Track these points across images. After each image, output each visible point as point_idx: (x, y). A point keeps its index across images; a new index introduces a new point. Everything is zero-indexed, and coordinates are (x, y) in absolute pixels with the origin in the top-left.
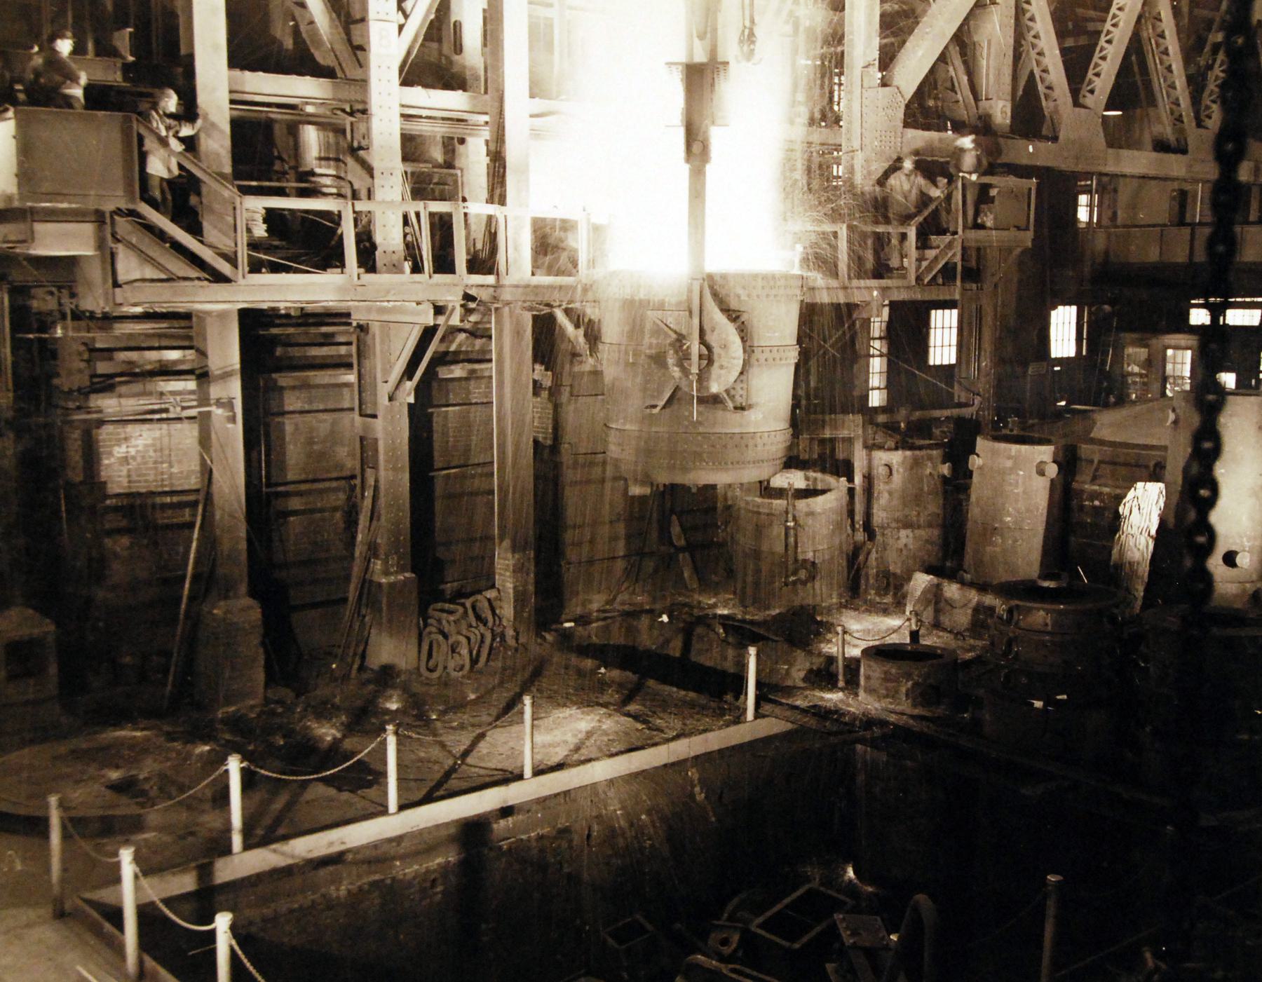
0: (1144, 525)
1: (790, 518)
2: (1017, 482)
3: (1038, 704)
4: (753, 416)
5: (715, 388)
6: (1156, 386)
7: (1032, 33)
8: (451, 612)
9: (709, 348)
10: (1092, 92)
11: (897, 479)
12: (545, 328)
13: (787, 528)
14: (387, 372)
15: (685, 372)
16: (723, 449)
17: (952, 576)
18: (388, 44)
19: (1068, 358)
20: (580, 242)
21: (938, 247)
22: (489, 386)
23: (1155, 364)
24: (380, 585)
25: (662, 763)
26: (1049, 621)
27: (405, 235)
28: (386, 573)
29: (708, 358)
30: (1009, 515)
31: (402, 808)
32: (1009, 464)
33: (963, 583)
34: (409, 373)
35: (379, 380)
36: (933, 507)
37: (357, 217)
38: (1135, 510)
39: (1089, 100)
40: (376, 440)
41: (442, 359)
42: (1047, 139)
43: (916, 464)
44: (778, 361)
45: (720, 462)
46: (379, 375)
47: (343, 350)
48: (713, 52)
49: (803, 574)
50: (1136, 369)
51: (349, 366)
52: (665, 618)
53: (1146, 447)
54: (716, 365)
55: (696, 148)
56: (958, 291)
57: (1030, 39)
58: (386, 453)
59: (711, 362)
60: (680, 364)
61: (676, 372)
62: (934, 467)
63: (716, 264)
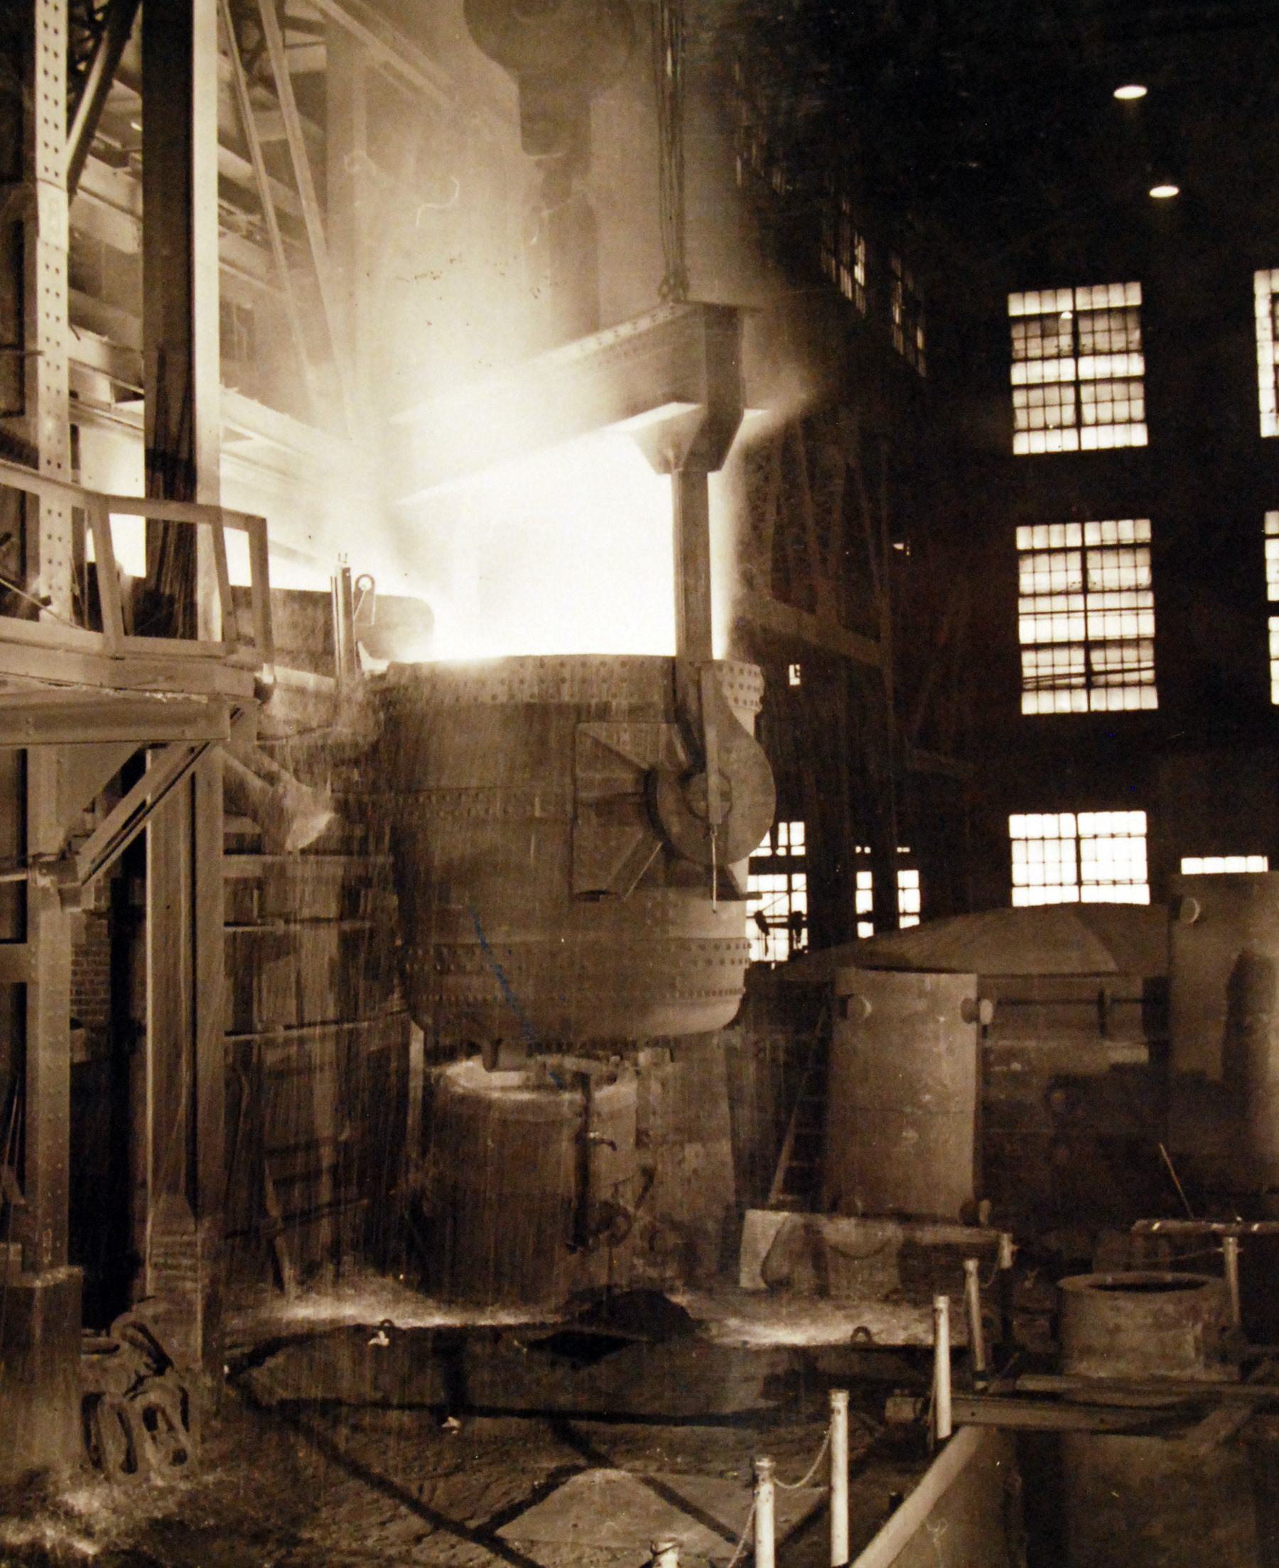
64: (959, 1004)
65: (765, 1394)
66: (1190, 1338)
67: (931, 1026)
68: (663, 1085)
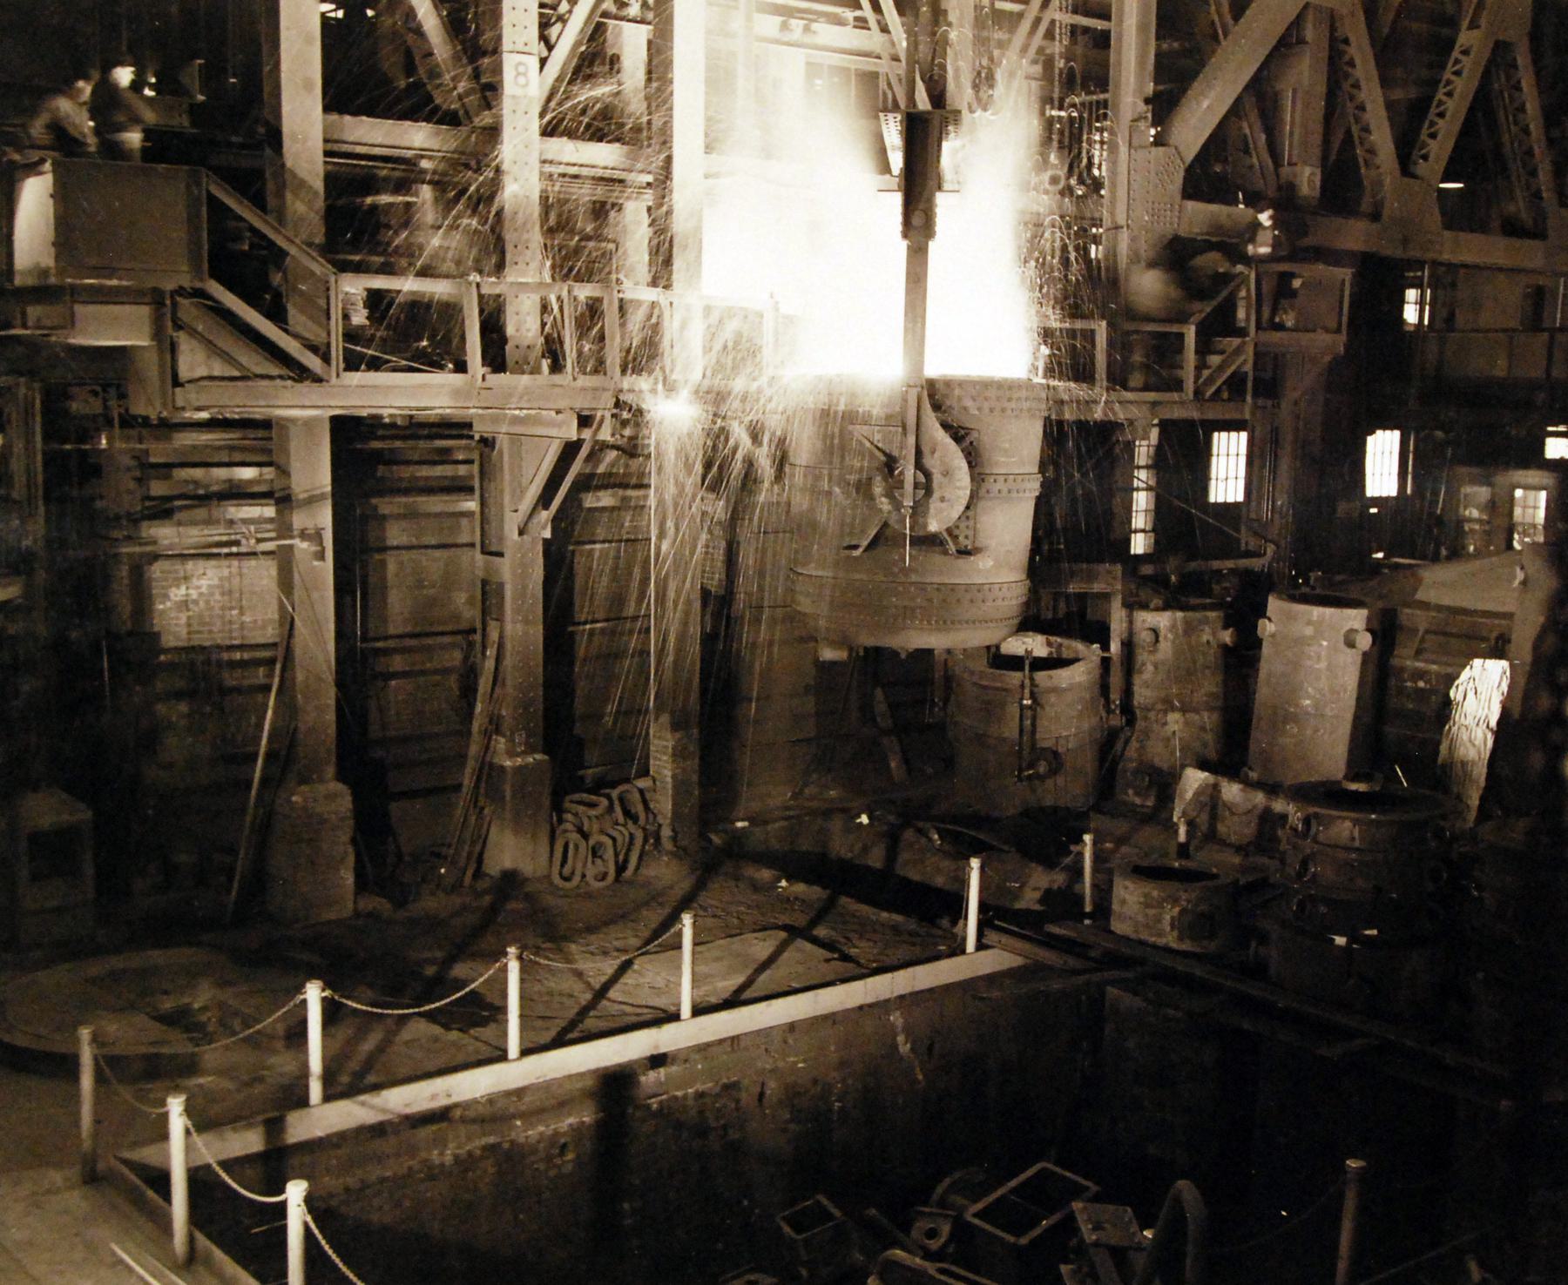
0: (1482, 714)
1: (1027, 691)
2: (1319, 654)
3: (1340, 941)
4: (984, 563)
5: (933, 526)
7: (1351, 81)
9: (928, 475)
13: (1022, 707)
14: (520, 492)
15: (897, 505)
16: (944, 605)
21: (1222, 352)
23: (1500, 509)
26: (1356, 834)
30: (1308, 697)
31: (525, 1052)
33: (1248, 784)
34: (545, 499)
36: (1209, 685)
38: (1471, 695)
41: (585, 483)
43: (1189, 628)
44: (1014, 495)
45: (945, 623)
47: (462, 470)
49: (1042, 768)
53: (1486, 614)
54: (936, 495)
55: (917, 220)
59: (929, 491)
60: (889, 494)
61: (884, 504)
62: (1214, 634)
63: (934, 369)
64: (1343, 632)
65: (1041, 901)
66: (1168, 917)
67: (1314, 648)
68: (1156, 668)
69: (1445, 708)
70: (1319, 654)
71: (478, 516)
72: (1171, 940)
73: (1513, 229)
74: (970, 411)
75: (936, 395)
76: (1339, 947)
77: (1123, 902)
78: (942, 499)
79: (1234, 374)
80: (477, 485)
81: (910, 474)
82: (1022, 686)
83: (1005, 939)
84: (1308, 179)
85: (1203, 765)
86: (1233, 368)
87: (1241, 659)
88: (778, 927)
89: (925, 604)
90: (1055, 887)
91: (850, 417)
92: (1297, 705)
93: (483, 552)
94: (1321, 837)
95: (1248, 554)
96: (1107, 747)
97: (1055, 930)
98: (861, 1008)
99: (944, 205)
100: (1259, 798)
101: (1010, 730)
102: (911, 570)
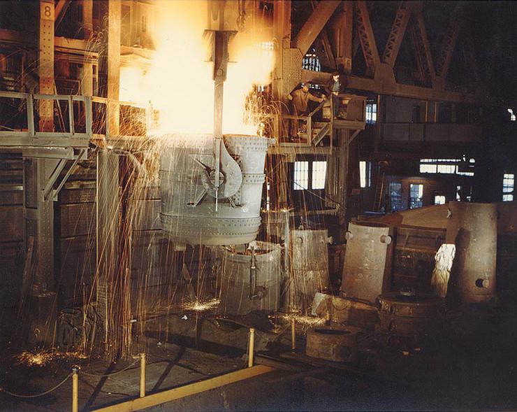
0: (445, 265)
1: (253, 264)
2: (370, 245)
3: (405, 353)
4: (244, 209)
5: (227, 195)
6: (406, 202)
7: (361, 26)
8: (75, 314)
9: (224, 174)
10: (388, 56)
11: (306, 244)
12: (123, 160)
13: (251, 269)
14: (43, 184)
15: (212, 186)
16: (230, 227)
17: (337, 294)
18: (49, 13)
19: (451, 174)
20: (147, 121)
21: (320, 128)
22: (93, 196)
23: (406, 193)
24: (38, 298)
25: (209, 389)
26: (411, 312)
27: (54, 112)
28: (41, 292)
29: (224, 179)
30: (367, 263)
31: (147, 394)
32: (367, 236)
33: (343, 298)
34: (55, 187)
35: (39, 190)
36: (325, 258)
37: (75, 104)
38: (442, 258)
39: (387, 59)
40: (36, 221)
41: (72, 179)
42: (367, 77)
43: (315, 237)
44: (256, 182)
45: (229, 234)
46: (39, 185)
47: (16, 173)
48: (222, 25)
49: (260, 294)
50: (395, 194)
51: (20, 182)
52: (185, 317)
53: (430, 229)
54: (228, 182)
55: (219, 73)
56: (331, 150)
57: (359, 29)
58: (42, 228)
59: (225, 181)
60: (209, 183)
61: (207, 186)
62: (324, 239)
63: (224, 132)
66: (332, 349)
69: (433, 263)
70: (370, 245)
71: (24, 193)
72: (333, 358)
73: (418, 83)
74: (238, 148)
75: (226, 142)
76: (405, 356)
77: (312, 344)
78: (231, 184)
79: (326, 136)
80: (24, 179)
81: (217, 173)
82: (251, 261)
83: (265, 360)
84: (347, 62)
85: (324, 291)
86: (325, 134)
87: (336, 251)
88: (165, 361)
89: (222, 227)
90: (272, 341)
91: (192, 151)
92: (363, 266)
93: (27, 208)
94: (397, 314)
95: (330, 208)
96: (283, 285)
97: (283, 356)
98: (210, 390)
99: (231, 69)
100: (348, 303)
101: (246, 280)
102: (217, 213)
